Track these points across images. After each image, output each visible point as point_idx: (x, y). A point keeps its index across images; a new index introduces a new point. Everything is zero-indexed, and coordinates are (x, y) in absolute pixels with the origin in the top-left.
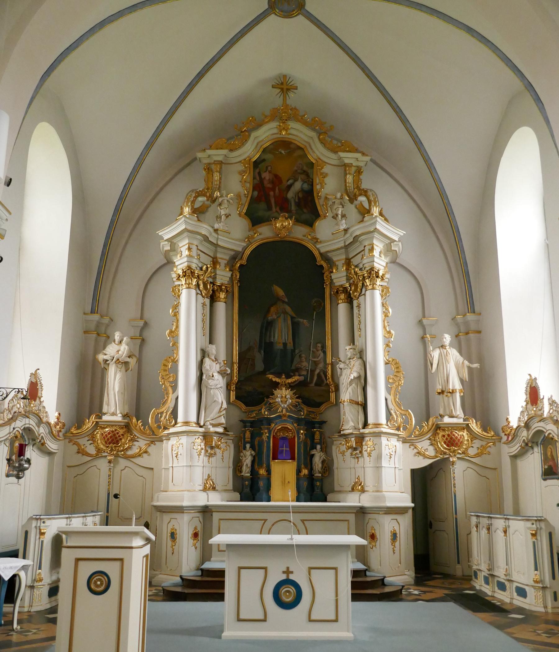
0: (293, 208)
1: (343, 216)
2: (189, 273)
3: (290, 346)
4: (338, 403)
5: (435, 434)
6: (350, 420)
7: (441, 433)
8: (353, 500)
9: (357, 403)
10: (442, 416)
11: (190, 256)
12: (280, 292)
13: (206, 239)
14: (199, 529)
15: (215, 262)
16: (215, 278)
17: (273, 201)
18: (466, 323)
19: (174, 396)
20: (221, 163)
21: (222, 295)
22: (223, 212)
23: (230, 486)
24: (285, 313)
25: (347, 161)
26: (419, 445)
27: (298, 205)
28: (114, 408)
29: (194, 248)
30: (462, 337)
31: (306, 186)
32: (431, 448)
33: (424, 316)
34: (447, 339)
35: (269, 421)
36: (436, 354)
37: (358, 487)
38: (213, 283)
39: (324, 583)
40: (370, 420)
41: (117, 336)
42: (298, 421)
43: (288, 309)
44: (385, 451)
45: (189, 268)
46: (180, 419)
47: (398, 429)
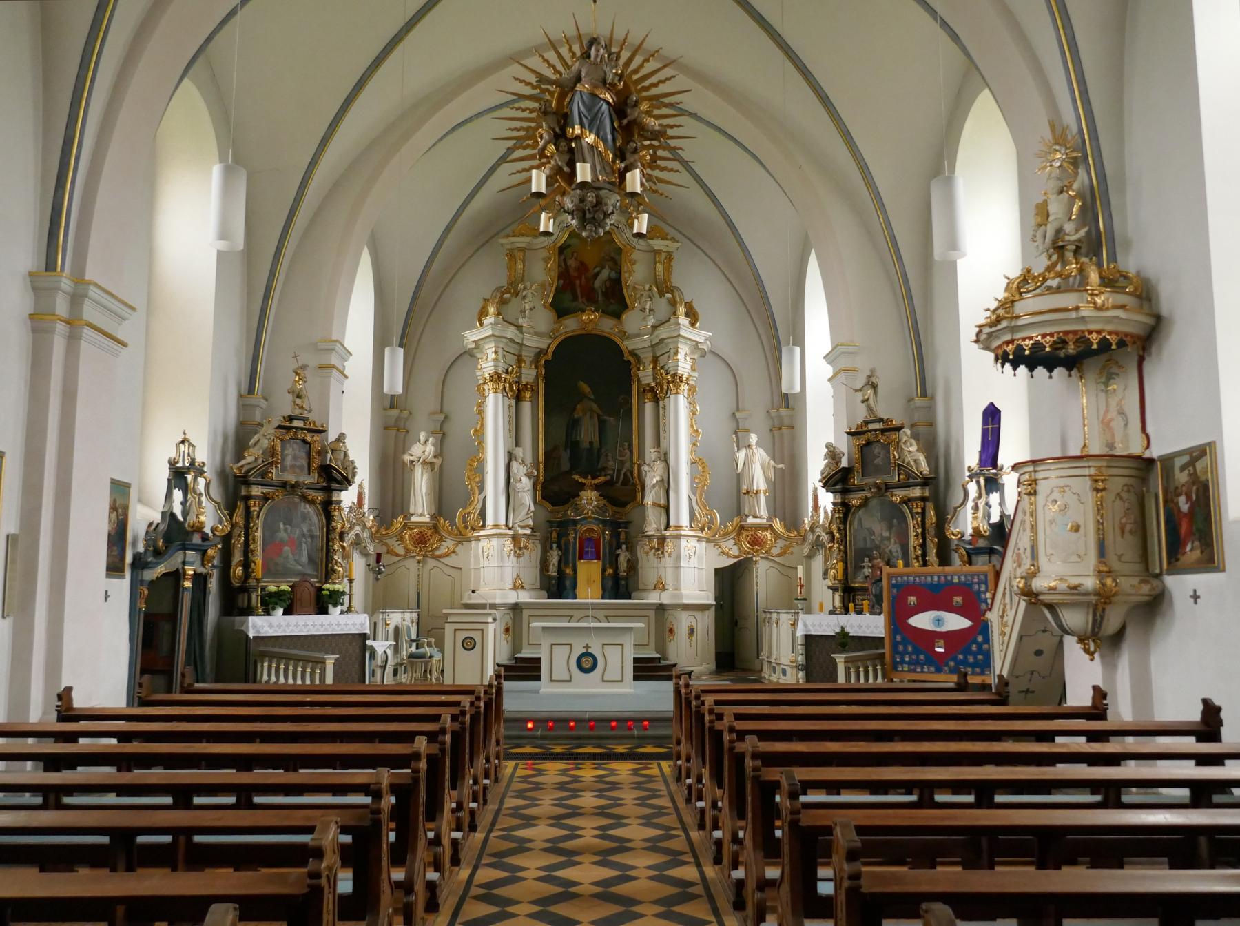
0: (600, 298)
1: (651, 310)
2: (496, 378)
3: (596, 444)
4: (642, 505)
5: (739, 534)
6: (652, 524)
7: (745, 533)
8: (654, 598)
9: (660, 506)
10: (747, 516)
11: (496, 360)
12: (586, 388)
13: (512, 340)
14: (510, 624)
15: (520, 360)
16: (520, 377)
17: (579, 291)
18: (780, 417)
19: (482, 496)
20: (523, 250)
21: (528, 395)
22: (527, 307)
23: (538, 585)
24: (592, 410)
25: (656, 248)
26: (724, 545)
27: (605, 294)
28: (421, 507)
29: (500, 351)
30: (776, 432)
31: (613, 274)
32: (735, 548)
33: (738, 410)
34: (754, 439)
35: (575, 522)
36: (741, 455)
37: (660, 586)
38: (518, 383)
39: (613, 654)
40: (672, 523)
41: (423, 436)
42: (604, 522)
43: (595, 406)
44: (684, 553)
45: (496, 373)
46: (490, 520)
47: (702, 529)
